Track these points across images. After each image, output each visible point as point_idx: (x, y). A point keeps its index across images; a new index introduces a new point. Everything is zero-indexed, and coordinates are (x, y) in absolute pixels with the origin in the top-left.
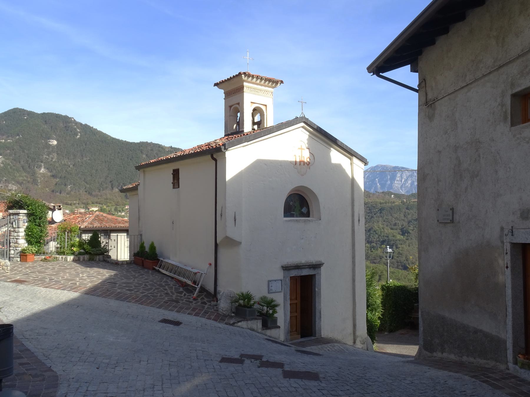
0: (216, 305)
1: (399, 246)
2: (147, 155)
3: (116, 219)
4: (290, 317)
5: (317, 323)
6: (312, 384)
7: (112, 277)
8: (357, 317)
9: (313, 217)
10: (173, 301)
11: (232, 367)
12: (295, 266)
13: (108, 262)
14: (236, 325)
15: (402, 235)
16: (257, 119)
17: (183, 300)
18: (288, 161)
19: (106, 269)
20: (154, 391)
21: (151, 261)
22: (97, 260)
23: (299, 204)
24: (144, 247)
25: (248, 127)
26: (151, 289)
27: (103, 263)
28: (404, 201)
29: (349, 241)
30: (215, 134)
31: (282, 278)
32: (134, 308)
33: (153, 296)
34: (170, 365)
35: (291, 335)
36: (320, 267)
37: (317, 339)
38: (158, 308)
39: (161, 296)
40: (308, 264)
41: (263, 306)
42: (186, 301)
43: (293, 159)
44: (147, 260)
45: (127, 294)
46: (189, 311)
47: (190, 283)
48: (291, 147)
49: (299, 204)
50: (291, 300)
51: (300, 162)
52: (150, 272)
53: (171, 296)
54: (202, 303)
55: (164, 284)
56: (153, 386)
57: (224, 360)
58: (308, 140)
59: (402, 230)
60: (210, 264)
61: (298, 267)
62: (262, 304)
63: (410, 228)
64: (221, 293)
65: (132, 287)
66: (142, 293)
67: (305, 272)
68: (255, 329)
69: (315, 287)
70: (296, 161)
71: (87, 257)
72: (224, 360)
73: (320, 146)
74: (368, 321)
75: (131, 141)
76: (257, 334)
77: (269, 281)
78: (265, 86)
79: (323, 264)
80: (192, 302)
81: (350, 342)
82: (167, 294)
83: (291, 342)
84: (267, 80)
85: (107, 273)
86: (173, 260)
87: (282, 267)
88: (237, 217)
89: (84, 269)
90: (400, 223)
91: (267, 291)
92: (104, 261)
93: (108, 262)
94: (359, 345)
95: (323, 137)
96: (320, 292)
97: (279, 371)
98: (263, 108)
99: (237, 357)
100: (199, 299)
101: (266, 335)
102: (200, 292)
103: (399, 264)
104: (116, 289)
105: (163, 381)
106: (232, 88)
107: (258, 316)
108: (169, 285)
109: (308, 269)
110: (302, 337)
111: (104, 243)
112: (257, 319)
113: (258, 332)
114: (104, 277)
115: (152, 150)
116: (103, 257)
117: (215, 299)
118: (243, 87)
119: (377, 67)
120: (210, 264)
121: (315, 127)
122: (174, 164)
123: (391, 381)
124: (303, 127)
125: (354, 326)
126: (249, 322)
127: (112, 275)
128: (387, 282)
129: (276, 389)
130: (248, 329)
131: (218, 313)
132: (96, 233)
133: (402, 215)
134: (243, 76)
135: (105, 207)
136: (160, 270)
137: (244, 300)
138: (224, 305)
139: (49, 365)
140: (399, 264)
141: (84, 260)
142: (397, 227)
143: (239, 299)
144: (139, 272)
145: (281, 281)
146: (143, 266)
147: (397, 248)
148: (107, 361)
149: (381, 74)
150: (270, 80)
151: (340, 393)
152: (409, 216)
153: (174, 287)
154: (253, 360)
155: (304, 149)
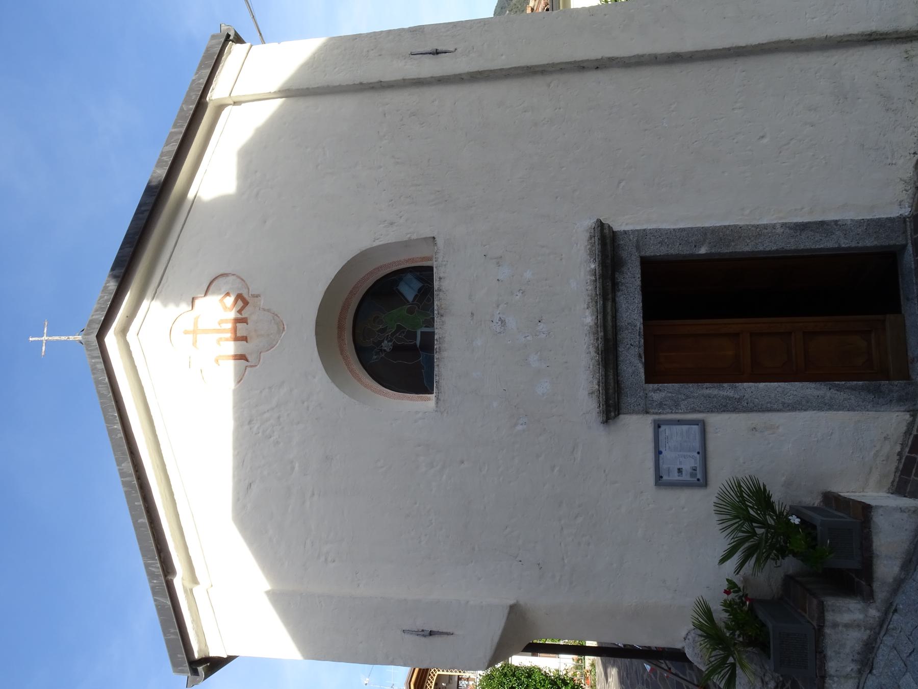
5: (845, 243)
18: (236, 392)
31: (649, 419)
36: (614, 234)
43: (229, 368)
51: (237, 339)
67: (631, 309)
73: (184, 249)
77: (659, 480)
79: (601, 225)
91: (697, 494)
96: (714, 230)
109: (621, 300)
121: (113, 286)
126: (832, 666)
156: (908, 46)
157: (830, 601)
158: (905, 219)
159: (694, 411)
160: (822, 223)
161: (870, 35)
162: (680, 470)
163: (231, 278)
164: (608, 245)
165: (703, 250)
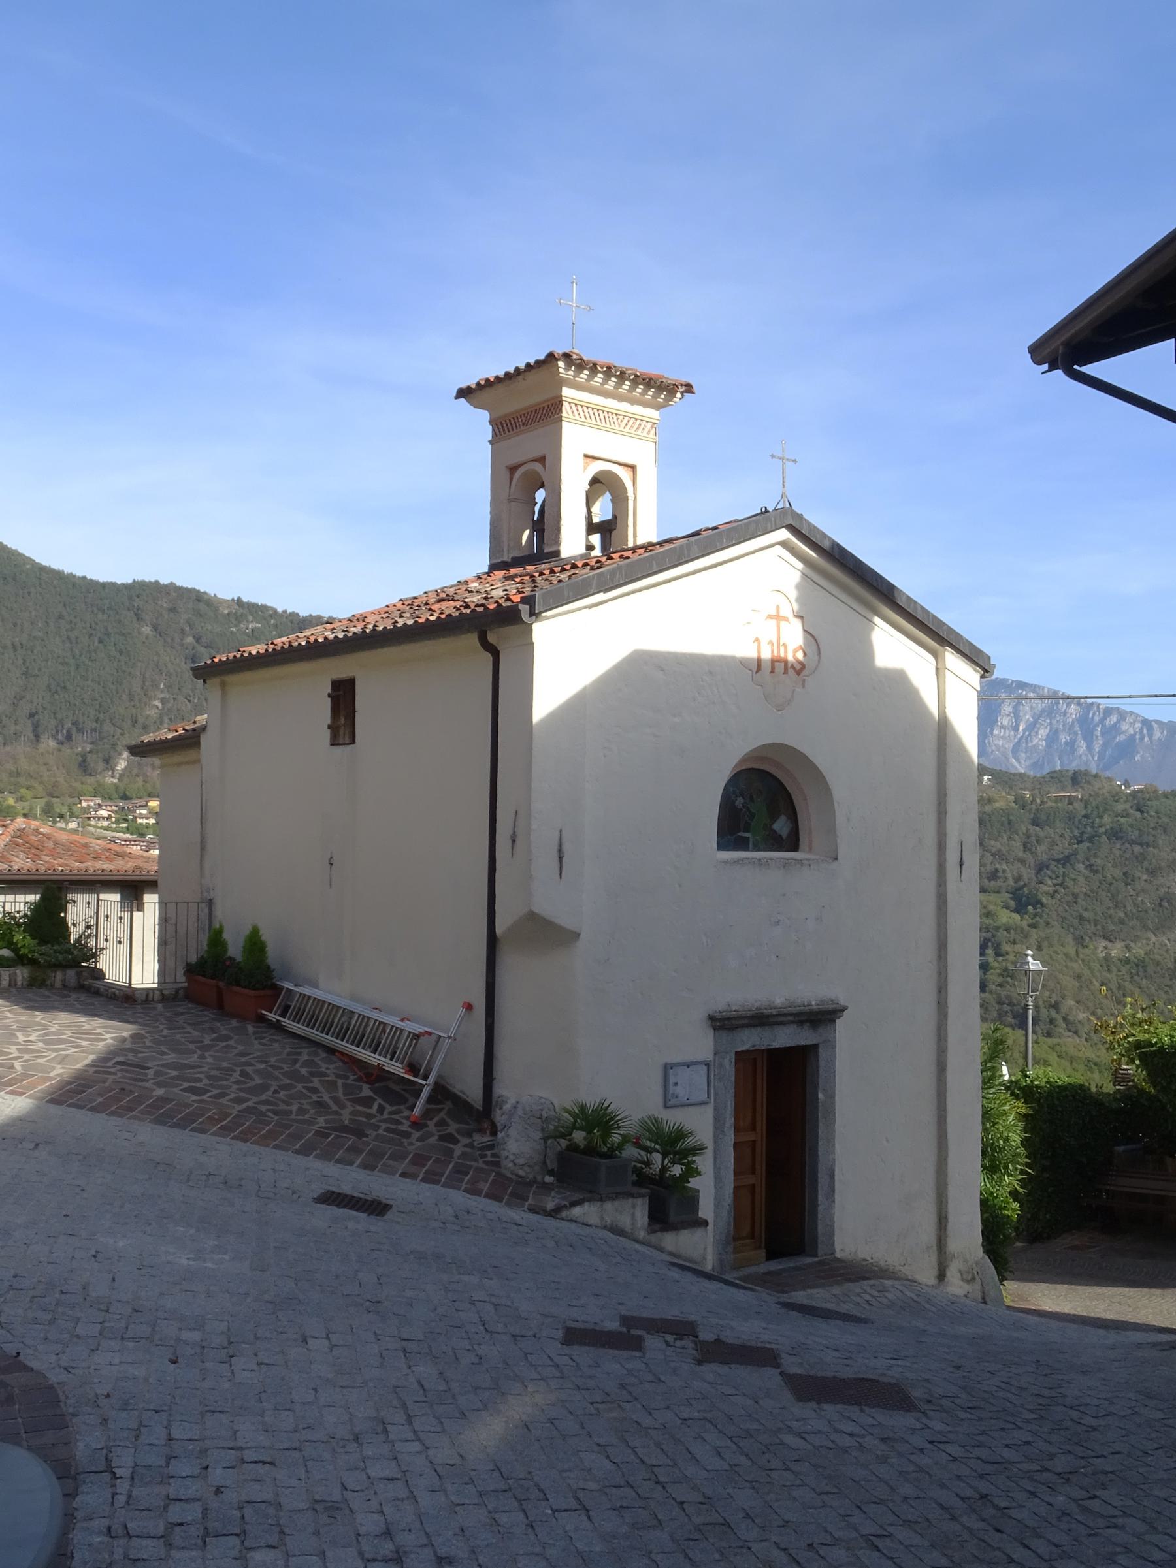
0: (491, 1147)
1: (1006, 947)
2: (155, 628)
3: (85, 846)
4: (736, 1188)
5: (820, 1209)
6: (900, 1421)
7: (128, 1045)
8: (952, 1192)
9: (810, 850)
10: (345, 1129)
11: (613, 1365)
12: (753, 1017)
13: (97, 993)
14: (564, 1214)
15: (1016, 911)
16: (602, 510)
17: (377, 1128)
18: (733, 658)
19: (98, 1016)
20: (393, 1443)
21: (252, 993)
22: (58, 984)
23: (765, 806)
24: (224, 945)
25: (573, 540)
26: (264, 1088)
27: (83, 997)
28: (1023, 797)
29: (928, 932)
30: (455, 560)
31: (710, 1057)
32: (223, 1153)
33: (276, 1113)
34: (404, 1350)
35: (736, 1251)
37: (821, 1263)
38: (297, 1152)
39: (301, 1111)
40: (794, 1010)
41: (649, 1151)
42: (387, 1130)
44: (235, 988)
45: (187, 1105)
46: (402, 1167)
47: (396, 1068)
48: (745, 609)
49: (765, 806)
50: (737, 1130)
52: (250, 1028)
53: (336, 1113)
54: (442, 1138)
55: (304, 1071)
56: (383, 1427)
57: (574, 1336)
58: (799, 587)
59: (1016, 894)
60: (469, 1007)
61: (761, 1019)
62: (648, 1143)
63: (1044, 888)
64: (507, 1107)
65: (200, 1080)
66: (239, 1101)
67: (785, 1038)
68: (628, 1228)
69: (816, 1088)
70: (759, 661)
71: (21, 974)
72: (574, 1336)
73: (839, 608)
74: (984, 1203)
75: (102, 578)
76: (637, 1246)
77: (668, 1067)
78: (633, 402)
80: (407, 1135)
81: (926, 1275)
82: (320, 1104)
83: (741, 1273)
84: (638, 379)
85: (107, 1029)
86: (331, 988)
87: (712, 1018)
88: (566, 847)
89: (25, 1016)
90: (1009, 870)
91: (659, 1100)
92: (81, 988)
93: (97, 993)
94: (956, 1286)
95: (848, 579)
96: (833, 1104)
97: (769, 1377)
98: (624, 475)
99: (613, 1325)
100: (431, 1124)
101: (661, 1250)
102: (430, 1100)
103: (1006, 1008)
104: (148, 1085)
105: (404, 1405)
106: (521, 409)
107: (634, 1184)
108: (325, 1075)
110: (771, 1255)
111: (80, 929)
112: (632, 1196)
113: (636, 1241)
114: (101, 1045)
115: (173, 610)
116: (79, 974)
117: (486, 1125)
118: (560, 403)
119: (1067, 344)
120: (469, 1007)
121: (826, 545)
122: (338, 666)
123: (1159, 1415)
124: (784, 544)
125: (942, 1220)
126: (608, 1205)
127: (124, 1040)
128: (1023, 1071)
129: (789, 1439)
130: (605, 1227)
131: (498, 1174)
132: (54, 893)
133: (1017, 844)
134: (561, 364)
135: (11, 801)
136: (285, 1021)
137: (590, 1132)
138: (519, 1146)
139: (10, 1349)
140: (1006, 1008)
141: (12, 983)
142: (999, 883)
143: (574, 1127)
144: (213, 1030)
145: (707, 1065)
146: (220, 1007)
147: (998, 954)
148: (196, 1336)
149: (1076, 367)
150: (648, 382)
151: (1007, 1453)
152: (1041, 848)
153: (340, 1082)
154: (670, 1338)
155: (786, 619)
156: (935, 1248)
157: (647, 1200)
158: (833, 1254)
159: (716, 1094)
160: (833, 1191)
161: (946, 1218)
162: (676, 1084)
163: (816, 658)
164: (822, 1017)
165: (820, 1096)
